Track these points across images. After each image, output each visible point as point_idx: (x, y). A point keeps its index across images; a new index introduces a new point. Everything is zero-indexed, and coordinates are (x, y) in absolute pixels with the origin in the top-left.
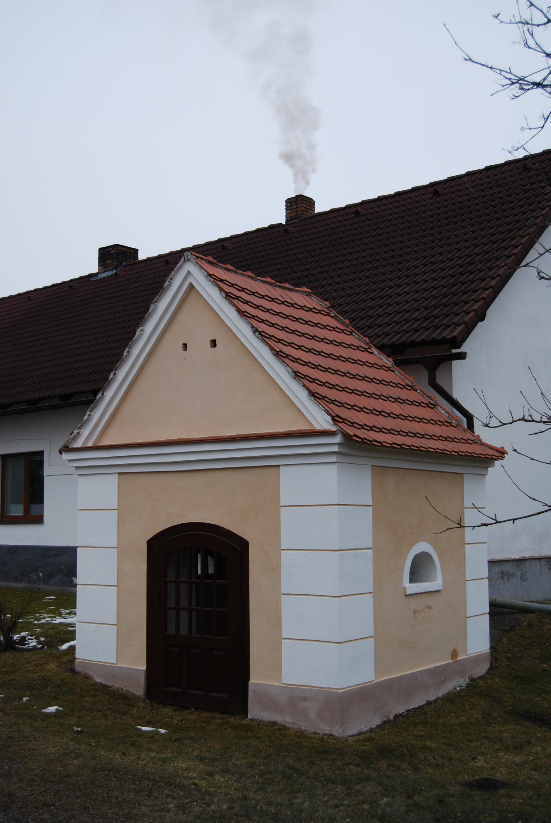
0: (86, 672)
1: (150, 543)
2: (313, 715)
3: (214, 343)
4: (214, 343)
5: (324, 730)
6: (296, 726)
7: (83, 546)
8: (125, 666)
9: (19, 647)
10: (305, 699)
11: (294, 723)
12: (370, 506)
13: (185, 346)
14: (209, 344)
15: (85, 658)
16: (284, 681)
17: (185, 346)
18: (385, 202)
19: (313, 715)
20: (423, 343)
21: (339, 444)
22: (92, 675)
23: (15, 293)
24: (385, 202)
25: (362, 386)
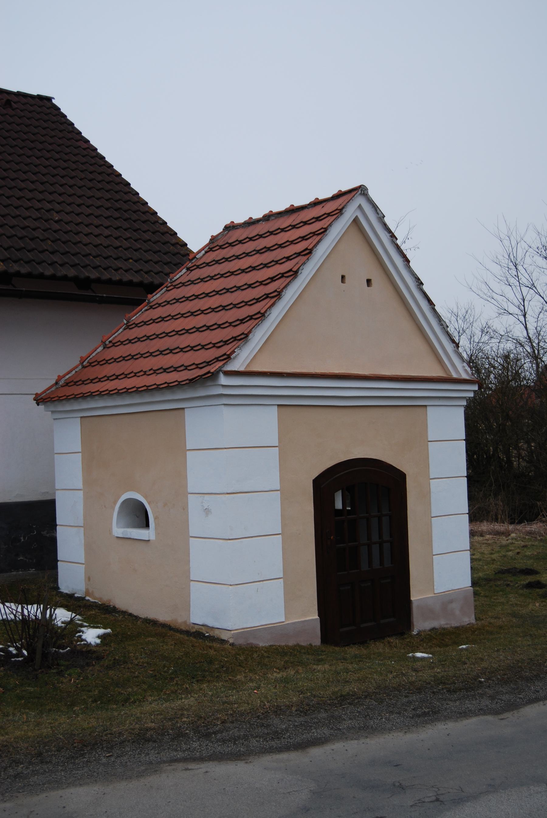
0: (249, 642)
1: (402, 476)
2: (457, 612)
3: (369, 282)
4: (369, 282)
5: (466, 622)
6: (449, 626)
7: (234, 491)
8: (297, 621)
9: (19, 660)
10: (451, 601)
11: (447, 624)
12: (56, 453)
13: (343, 277)
14: (347, 279)
15: (245, 626)
16: (436, 592)
17: (343, 277)
18: (24, 100)
19: (457, 612)
20: (120, 283)
21: (475, 391)
22: (258, 643)
23: (85, 134)
24: (24, 100)
25: (178, 325)
